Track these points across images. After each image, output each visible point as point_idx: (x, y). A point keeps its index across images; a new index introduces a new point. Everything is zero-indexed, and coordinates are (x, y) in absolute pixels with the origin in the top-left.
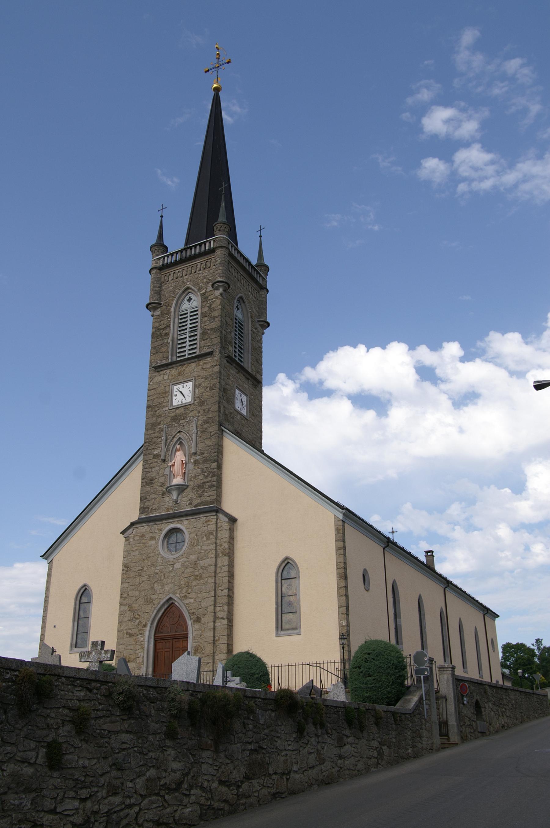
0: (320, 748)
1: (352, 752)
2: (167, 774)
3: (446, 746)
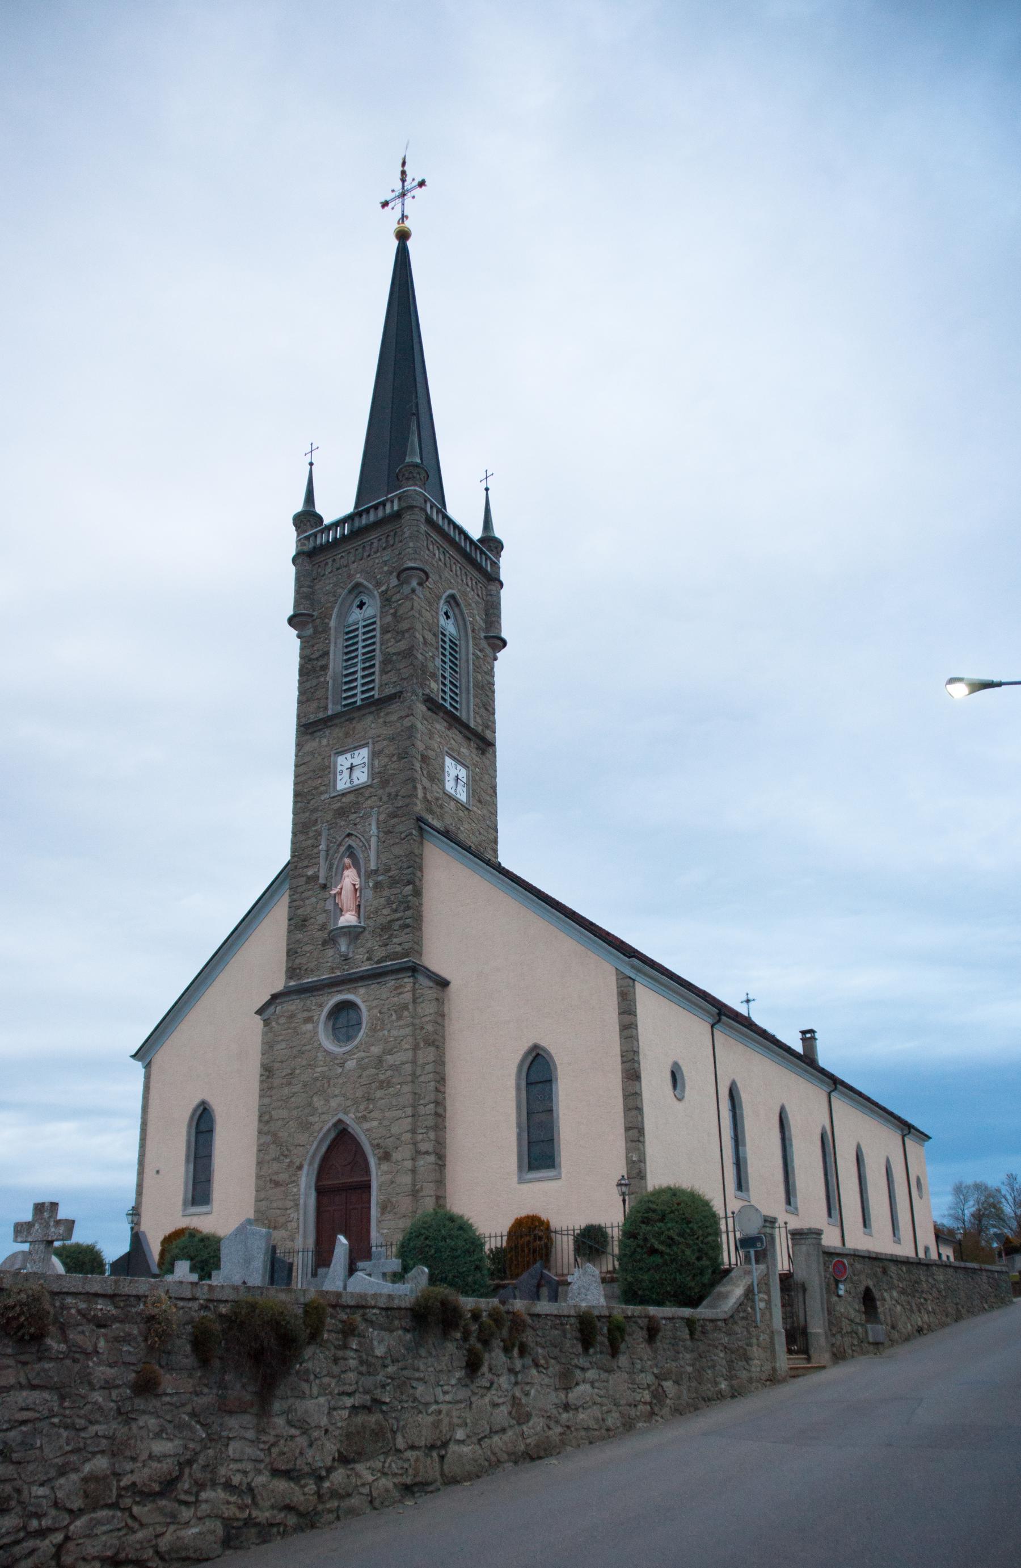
0: (518, 1394)
1: (594, 1396)
2: (140, 1465)
3: (800, 1372)
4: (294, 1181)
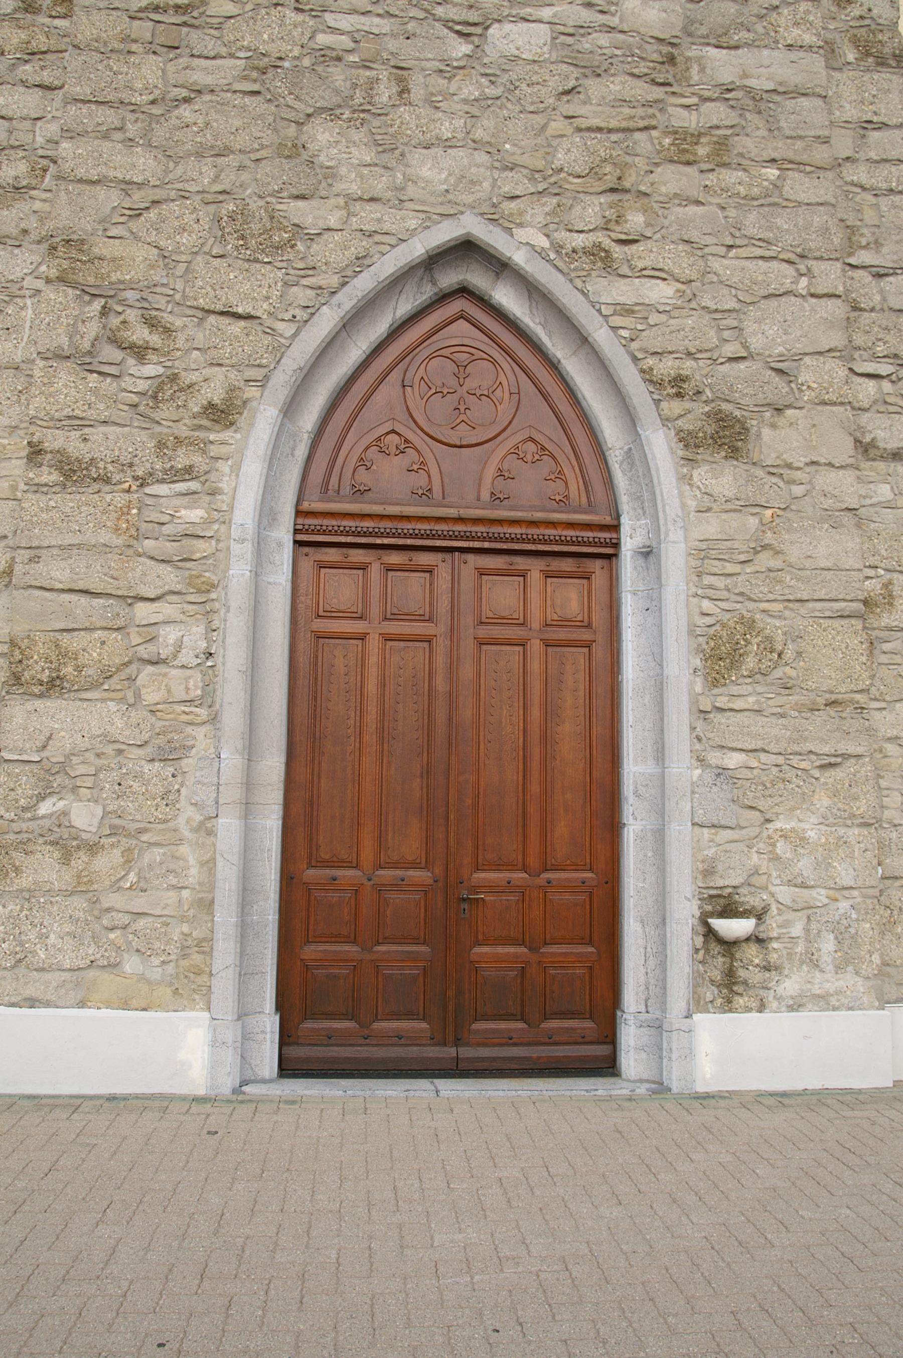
4: (188, 472)
